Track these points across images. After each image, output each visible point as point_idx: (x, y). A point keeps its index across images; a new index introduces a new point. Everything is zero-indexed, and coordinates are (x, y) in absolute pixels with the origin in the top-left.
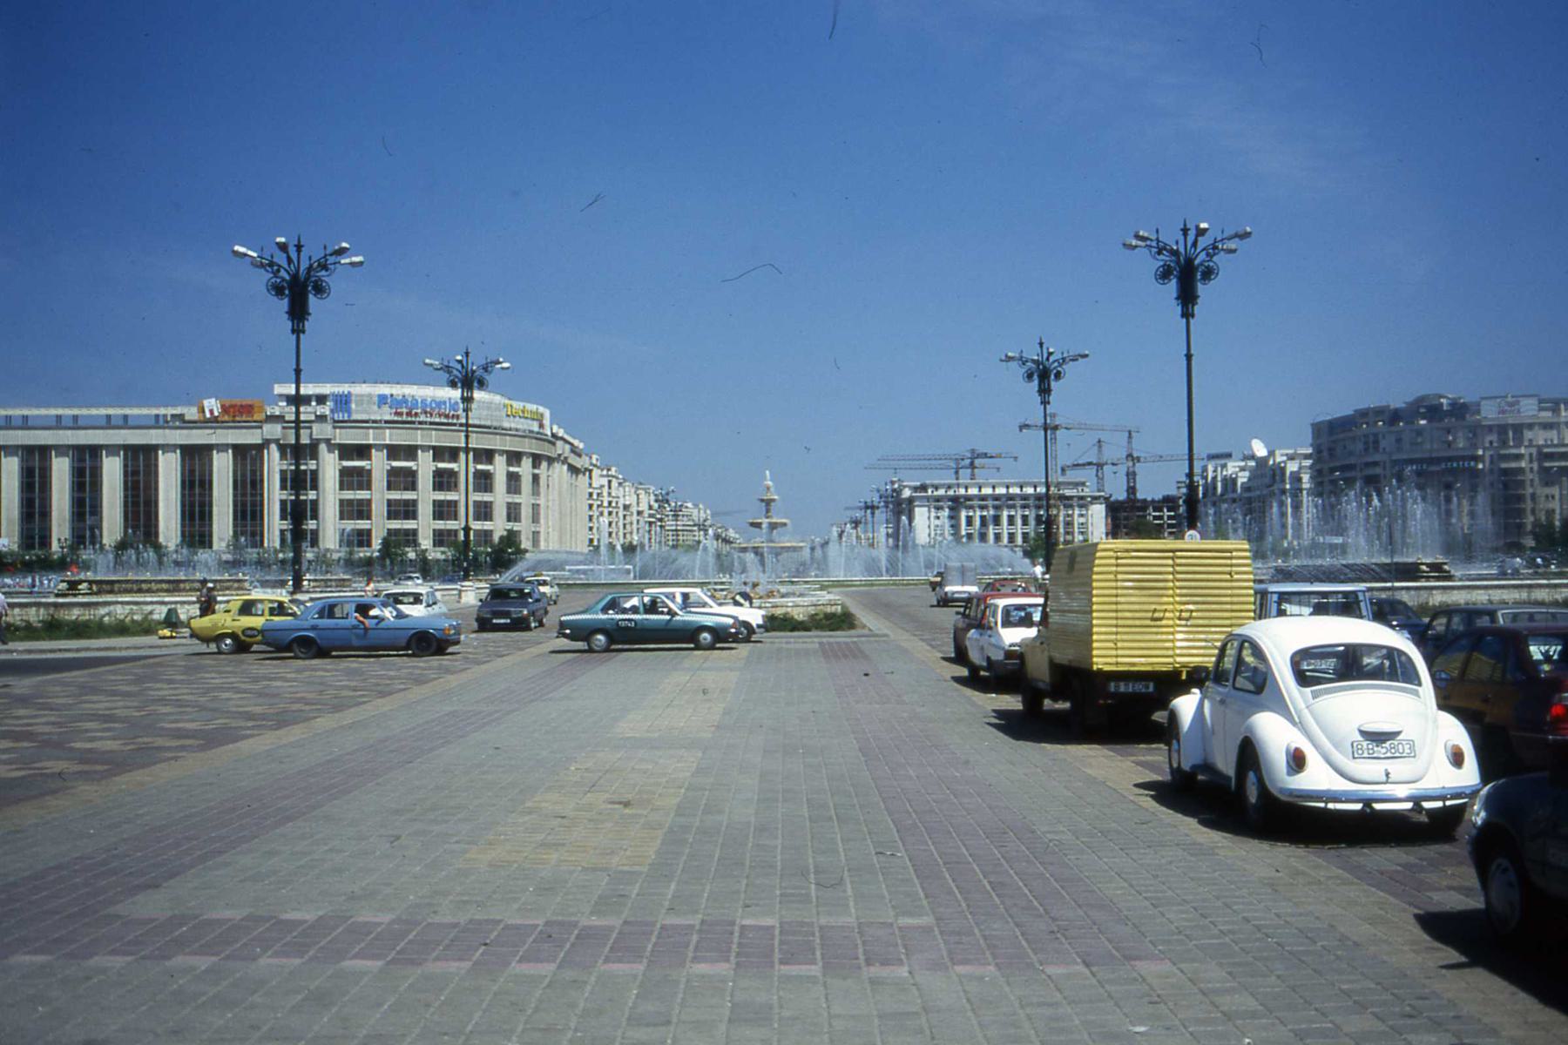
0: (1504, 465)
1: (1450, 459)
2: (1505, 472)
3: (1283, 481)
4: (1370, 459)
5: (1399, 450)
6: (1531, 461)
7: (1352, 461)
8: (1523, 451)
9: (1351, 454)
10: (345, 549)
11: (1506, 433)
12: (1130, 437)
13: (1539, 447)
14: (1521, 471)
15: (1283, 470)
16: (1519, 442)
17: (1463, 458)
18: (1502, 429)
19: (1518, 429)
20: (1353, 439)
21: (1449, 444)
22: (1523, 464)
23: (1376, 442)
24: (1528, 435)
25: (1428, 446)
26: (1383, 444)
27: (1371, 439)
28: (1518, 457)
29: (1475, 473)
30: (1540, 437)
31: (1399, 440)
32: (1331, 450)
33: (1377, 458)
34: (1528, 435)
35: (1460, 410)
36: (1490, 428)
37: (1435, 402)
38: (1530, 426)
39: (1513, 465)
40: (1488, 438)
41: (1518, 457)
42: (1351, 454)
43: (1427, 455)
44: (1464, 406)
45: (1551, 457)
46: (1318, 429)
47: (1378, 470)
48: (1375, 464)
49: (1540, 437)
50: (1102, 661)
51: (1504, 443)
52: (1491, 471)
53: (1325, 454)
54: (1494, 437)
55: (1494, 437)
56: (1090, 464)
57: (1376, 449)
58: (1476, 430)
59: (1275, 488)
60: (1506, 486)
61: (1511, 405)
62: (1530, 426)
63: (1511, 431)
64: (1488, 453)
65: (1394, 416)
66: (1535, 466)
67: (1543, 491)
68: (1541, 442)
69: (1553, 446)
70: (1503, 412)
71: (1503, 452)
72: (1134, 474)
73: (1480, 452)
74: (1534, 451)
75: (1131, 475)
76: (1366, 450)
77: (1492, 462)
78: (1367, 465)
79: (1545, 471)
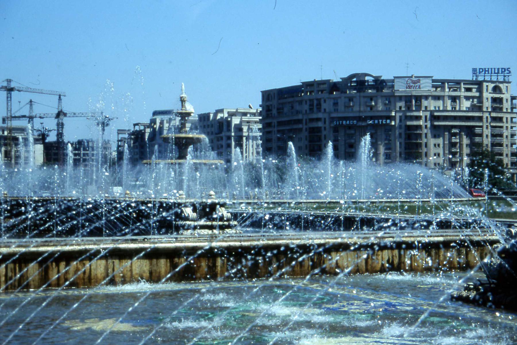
0: (409, 123)
1: (371, 118)
2: (409, 127)
3: (229, 130)
4: (315, 116)
5: (336, 110)
6: (426, 121)
7: (300, 117)
8: (421, 114)
9: (298, 112)
10: (19, 149)
11: (411, 102)
12: (60, 97)
13: (432, 112)
14: (419, 127)
15: (229, 123)
16: (419, 108)
17: (382, 117)
18: (408, 99)
19: (419, 99)
20: (300, 102)
21: (371, 107)
22: (421, 123)
23: (319, 105)
24: (425, 103)
25: (356, 108)
26: (324, 106)
27: (315, 102)
28: (418, 118)
29: (389, 128)
30: (432, 105)
31: (336, 104)
32: (280, 111)
33: (320, 115)
34: (425, 103)
35: (379, 84)
36: (400, 98)
37: (362, 79)
38: (426, 97)
39: (415, 123)
40: (399, 104)
41: (418, 118)
42: (298, 112)
43: (357, 115)
44: (383, 81)
45: (438, 118)
46: (267, 96)
47: (320, 124)
48: (318, 120)
49: (432, 105)
50: (386, 251)
51: (409, 108)
52: (400, 127)
53: (274, 112)
54: (402, 104)
55: (402, 104)
56: (24, 116)
57: (319, 110)
58: (392, 98)
59: (223, 134)
60: (409, 137)
61: (414, 82)
62: (426, 97)
63: (414, 101)
64: (398, 115)
65: (334, 87)
66: (429, 124)
67: (432, 141)
68: (432, 108)
69: (439, 111)
70: (410, 87)
71: (409, 114)
72: (62, 124)
73: (393, 114)
74: (428, 114)
75: (60, 126)
76: (311, 110)
77: (400, 121)
78: (312, 120)
79: (434, 127)
